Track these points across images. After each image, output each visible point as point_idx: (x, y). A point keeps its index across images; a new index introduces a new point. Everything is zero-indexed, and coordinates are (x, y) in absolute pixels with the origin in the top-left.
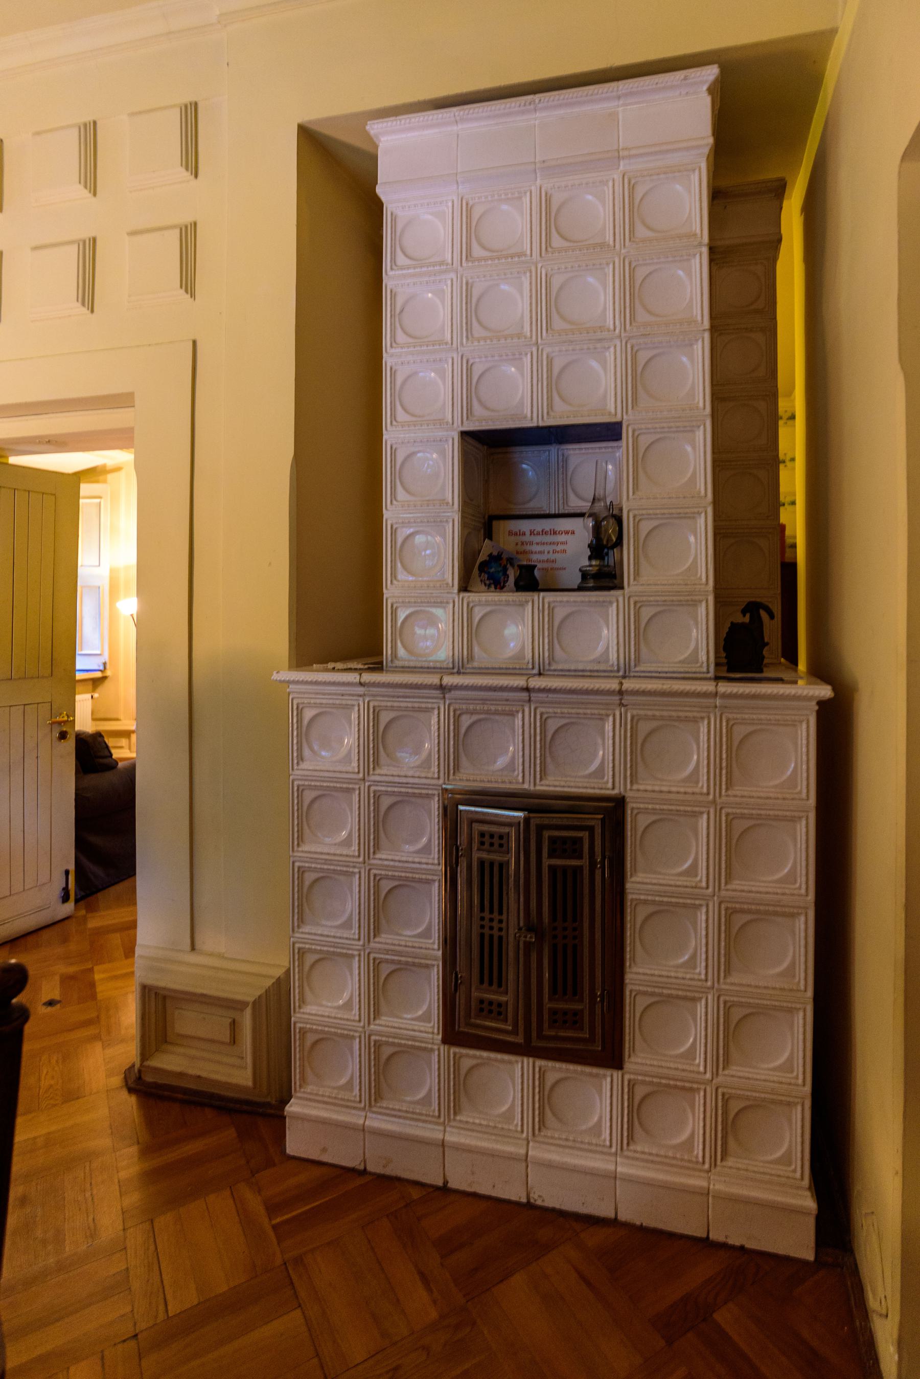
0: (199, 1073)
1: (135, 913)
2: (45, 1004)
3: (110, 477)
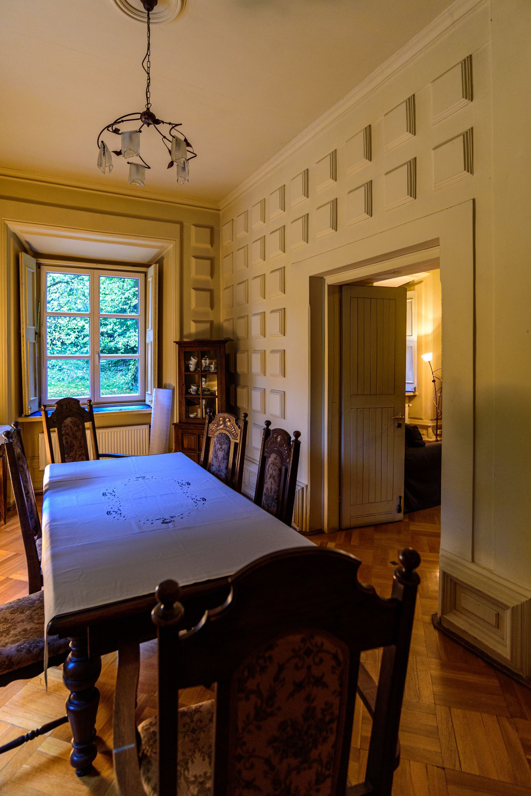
0: (476, 636)
1: (440, 529)
2: (391, 562)
3: (416, 287)
